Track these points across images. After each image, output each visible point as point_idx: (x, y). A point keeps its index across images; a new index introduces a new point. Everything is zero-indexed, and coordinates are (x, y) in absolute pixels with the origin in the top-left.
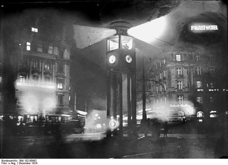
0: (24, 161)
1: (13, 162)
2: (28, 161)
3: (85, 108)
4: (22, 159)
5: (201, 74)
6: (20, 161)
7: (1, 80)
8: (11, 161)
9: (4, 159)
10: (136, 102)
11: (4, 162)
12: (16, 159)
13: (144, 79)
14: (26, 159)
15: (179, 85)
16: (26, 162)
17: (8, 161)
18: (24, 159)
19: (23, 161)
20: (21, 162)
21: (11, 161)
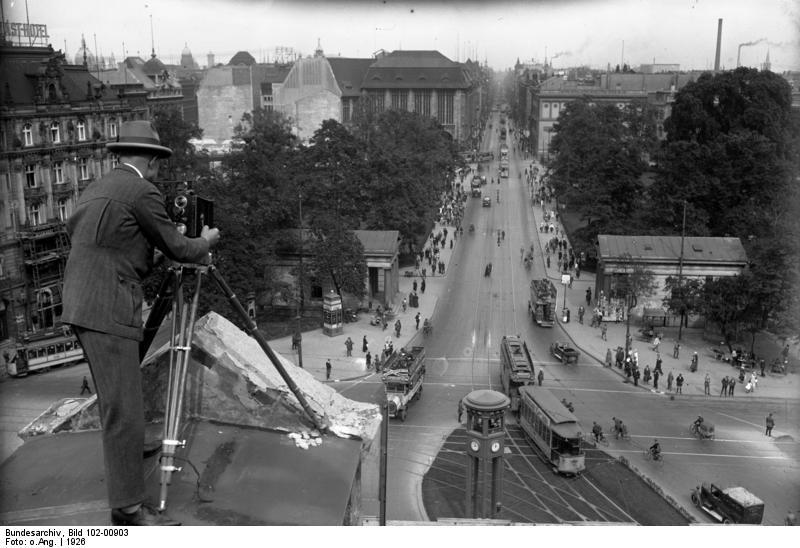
1: (45, 538)
2: (97, 533)
4: (79, 528)
6: (71, 532)
8: (39, 534)
9: (13, 529)
11: (14, 538)
14: (90, 528)
17: (28, 533)
21: (39, 534)
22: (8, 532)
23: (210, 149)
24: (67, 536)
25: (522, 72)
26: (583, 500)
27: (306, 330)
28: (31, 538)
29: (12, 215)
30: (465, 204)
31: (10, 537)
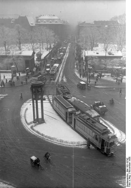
0: (127, 168)
1: (129, 178)
2: (127, 165)
3: (75, 41)
4: (126, 169)
5: (11, 71)
6: (127, 171)
7: (5, 186)
8: (128, 179)
9: (126, 185)
10: (33, 42)
11: (129, 185)
12: (126, 174)
13: (82, 113)
14: (126, 167)
15: (109, 146)
16: (129, 166)
17: (128, 181)
18: (126, 168)
19: (128, 169)
20: (129, 171)
21: (128, 179)
22: (127, 186)
23: (62, 122)
24: (128, 172)
25: (112, 141)
26: (87, 105)
27: (38, 117)
28: (129, 181)
29: (41, 137)
30: (113, 153)
31: (128, 186)
